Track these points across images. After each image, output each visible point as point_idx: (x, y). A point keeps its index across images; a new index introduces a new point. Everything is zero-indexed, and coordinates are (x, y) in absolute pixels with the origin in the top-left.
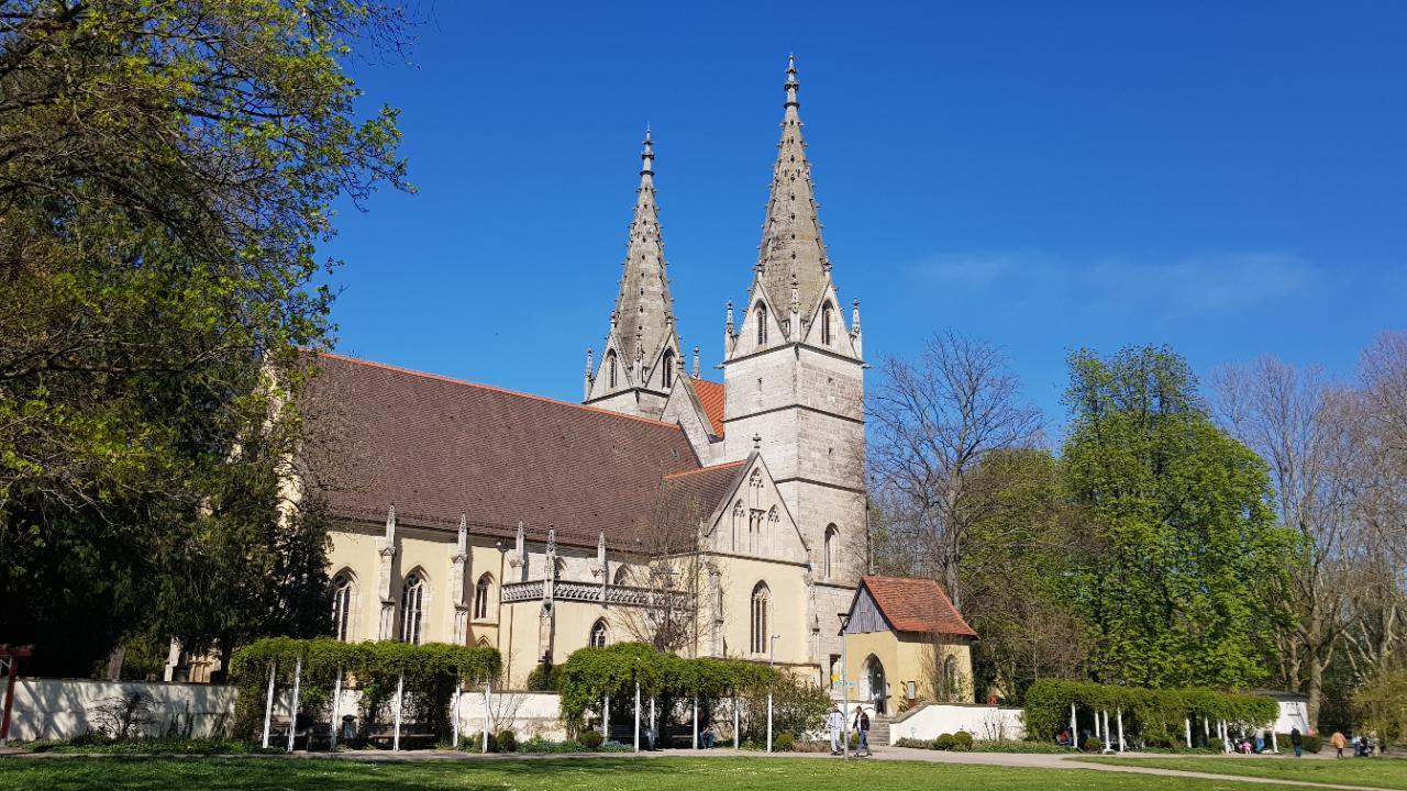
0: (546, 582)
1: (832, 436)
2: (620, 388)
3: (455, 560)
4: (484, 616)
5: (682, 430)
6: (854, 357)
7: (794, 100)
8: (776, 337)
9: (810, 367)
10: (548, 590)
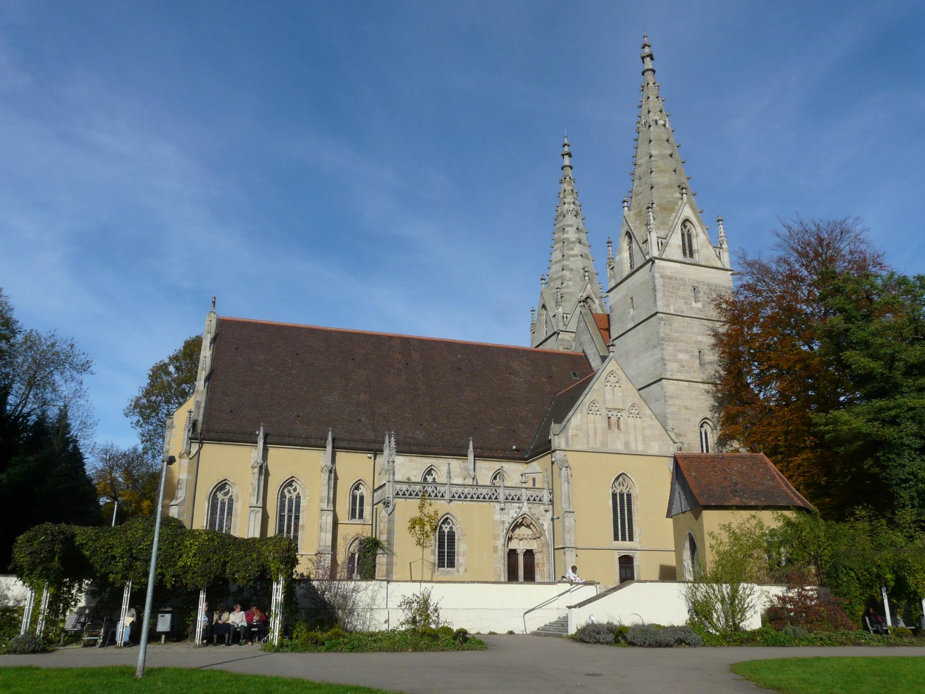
3: (253, 467)
4: (631, 539)
5: (586, 356)
6: (720, 266)
9: (670, 278)
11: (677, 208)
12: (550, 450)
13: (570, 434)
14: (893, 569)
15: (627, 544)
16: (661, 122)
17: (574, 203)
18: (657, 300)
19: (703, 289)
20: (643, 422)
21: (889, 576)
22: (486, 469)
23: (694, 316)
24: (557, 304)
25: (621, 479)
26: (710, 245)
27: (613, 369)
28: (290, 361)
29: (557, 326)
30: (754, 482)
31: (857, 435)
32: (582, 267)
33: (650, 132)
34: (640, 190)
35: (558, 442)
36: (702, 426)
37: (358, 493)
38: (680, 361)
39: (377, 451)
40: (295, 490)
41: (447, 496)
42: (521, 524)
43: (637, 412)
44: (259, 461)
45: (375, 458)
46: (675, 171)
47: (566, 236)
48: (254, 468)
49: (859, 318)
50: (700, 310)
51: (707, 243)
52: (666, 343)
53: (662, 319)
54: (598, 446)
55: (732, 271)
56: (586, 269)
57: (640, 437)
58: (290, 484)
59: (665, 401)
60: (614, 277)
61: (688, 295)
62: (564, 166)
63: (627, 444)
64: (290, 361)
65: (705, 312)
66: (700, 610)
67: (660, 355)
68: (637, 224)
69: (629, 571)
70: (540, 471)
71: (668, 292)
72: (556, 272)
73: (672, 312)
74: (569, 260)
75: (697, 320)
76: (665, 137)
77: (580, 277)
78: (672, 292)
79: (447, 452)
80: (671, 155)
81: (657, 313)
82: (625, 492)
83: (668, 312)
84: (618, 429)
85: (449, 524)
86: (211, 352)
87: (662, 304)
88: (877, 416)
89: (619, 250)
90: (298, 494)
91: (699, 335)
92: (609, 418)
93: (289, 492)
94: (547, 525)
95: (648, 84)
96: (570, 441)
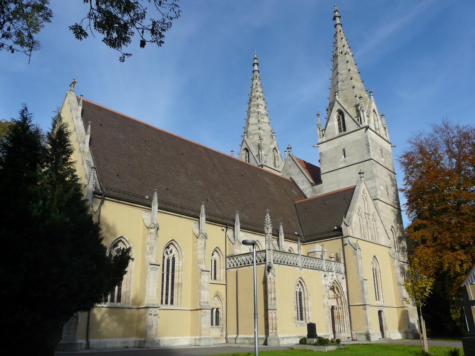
0: (267, 251)
5: (293, 182)
13: (353, 227)
34: (344, 88)
47: (259, 110)
48: (151, 228)
52: (376, 178)
58: (168, 247)
72: (254, 130)
77: (269, 136)
81: (371, 159)
86: (82, 122)
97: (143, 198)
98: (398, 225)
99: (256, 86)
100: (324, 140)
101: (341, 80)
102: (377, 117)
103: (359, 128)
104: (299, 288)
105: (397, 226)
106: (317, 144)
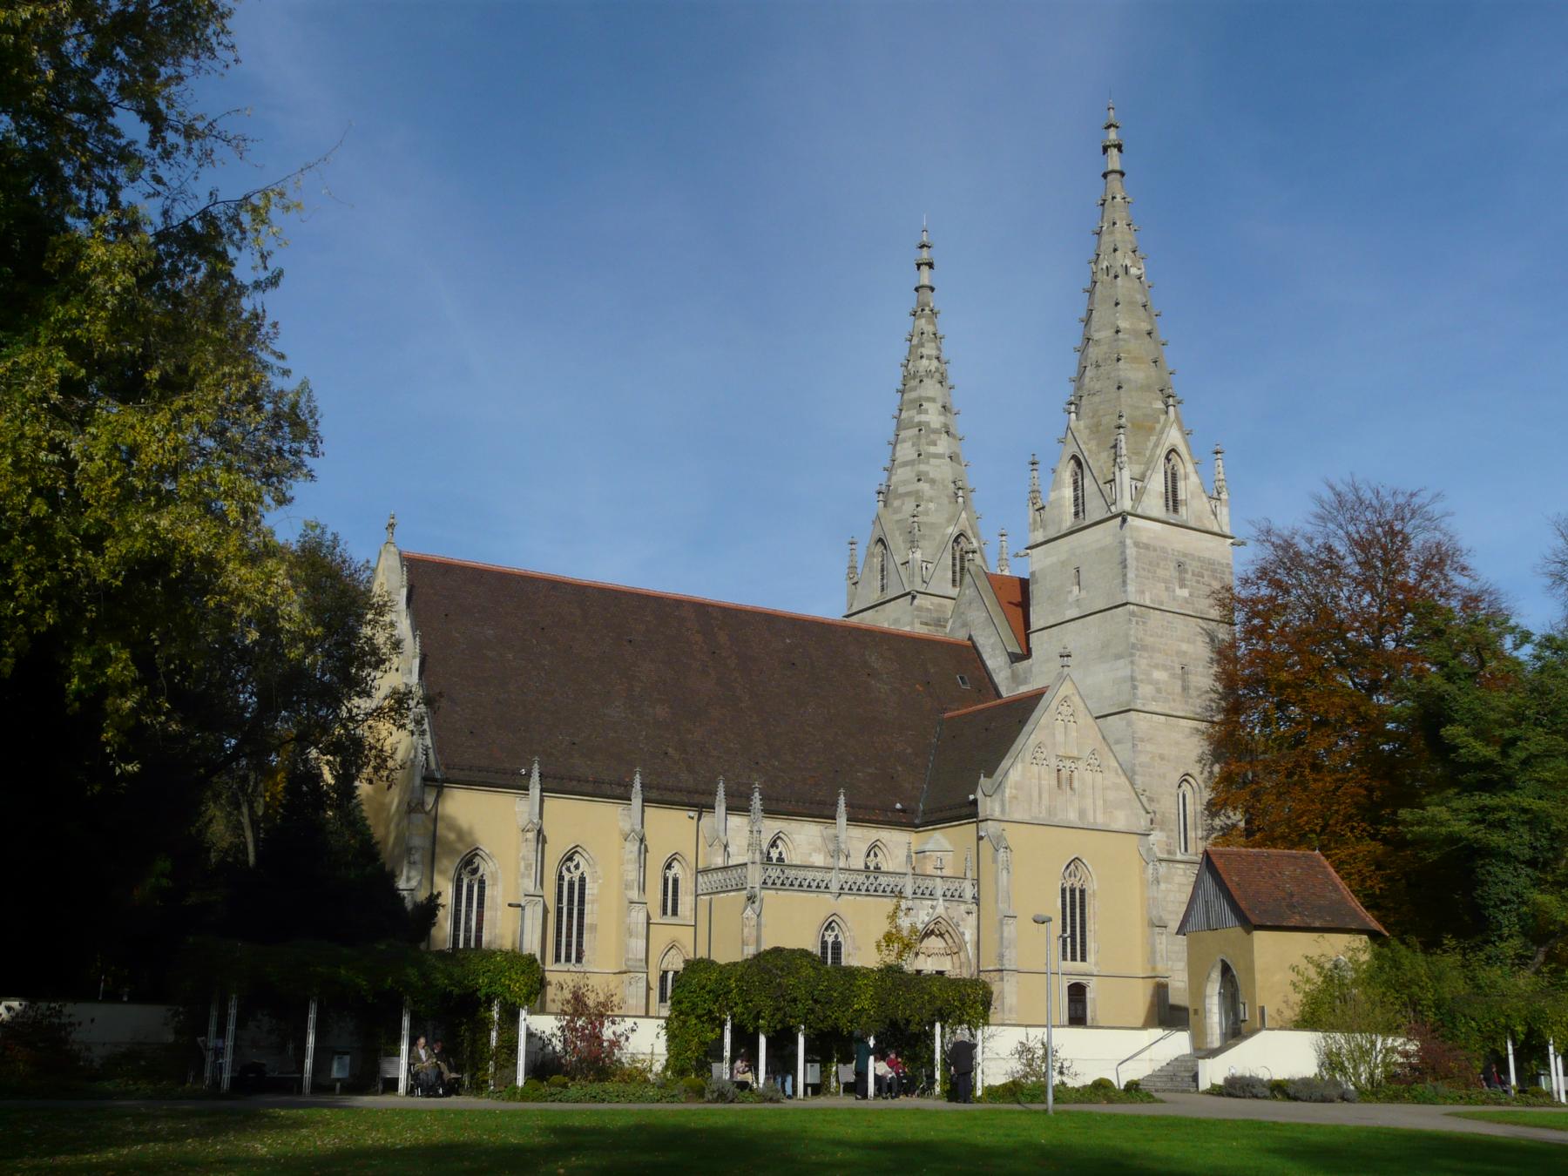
0: (750, 866)
1: (1184, 647)
2: (891, 593)
4: (1083, 959)
5: (975, 647)
6: (1216, 529)
7: (1118, 167)
8: (1095, 510)
9: (1147, 547)
10: (755, 876)
11: (1158, 427)
12: (976, 817)
14: (1525, 1019)
15: (1078, 965)
16: (1133, 271)
17: (938, 358)
18: (1128, 581)
19: (1192, 566)
20: (1103, 779)
21: (1519, 1028)
22: (857, 839)
23: (1178, 611)
24: (913, 544)
25: (1072, 866)
26: (1203, 495)
27: (1067, 693)
28: (535, 642)
29: (911, 582)
30: (1313, 894)
31: (1452, 839)
32: (951, 479)
33: (1116, 286)
34: (1098, 386)
35: (987, 806)
36: (1179, 786)
37: (670, 874)
38: (1155, 683)
39: (702, 806)
40: (577, 867)
41: (834, 888)
42: (932, 932)
43: (1097, 763)
44: (535, 821)
45: (699, 819)
46: (1155, 362)
47: (923, 418)
48: (528, 831)
49: (1462, 677)
50: (1186, 600)
51: (1200, 490)
52: (1138, 653)
53: (1133, 614)
54: (1043, 816)
55: (1232, 538)
56: (960, 484)
57: (1100, 803)
58: (570, 859)
59: (1134, 746)
60: (1044, 526)
61: (1171, 576)
62: (922, 287)
63: (1082, 813)
64: (535, 642)
65: (1193, 604)
66: (1331, 1062)
67: (1128, 672)
68: (1093, 445)
69: (1079, 1007)
70: (949, 847)
71: (1144, 569)
72: (905, 483)
73: (1148, 603)
74: (928, 463)
75: (1182, 617)
76: (1140, 298)
77: (948, 496)
78: (1149, 571)
79: (805, 811)
80: (1149, 334)
82: (1078, 886)
83: (1142, 602)
84: (1071, 788)
85: (833, 930)
86: (409, 622)
87: (1134, 589)
88: (1483, 816)
89: (1057, 485)
90: (582, 874)
91: (1182, 641)
92: (1059, 770)
93: (568, 870)
94: (969, 936)
95: (1114, 198)
96: (1007, 807)
97: (516, 773)
98: (1217, 768)
99: (921, 339)
100: (1039, 536)
101: (1094, 359)
102: (1185, 467)
103: (1109, 515)
104: (834, 933)
105: (1211, 772)
106: (1027, 549)
